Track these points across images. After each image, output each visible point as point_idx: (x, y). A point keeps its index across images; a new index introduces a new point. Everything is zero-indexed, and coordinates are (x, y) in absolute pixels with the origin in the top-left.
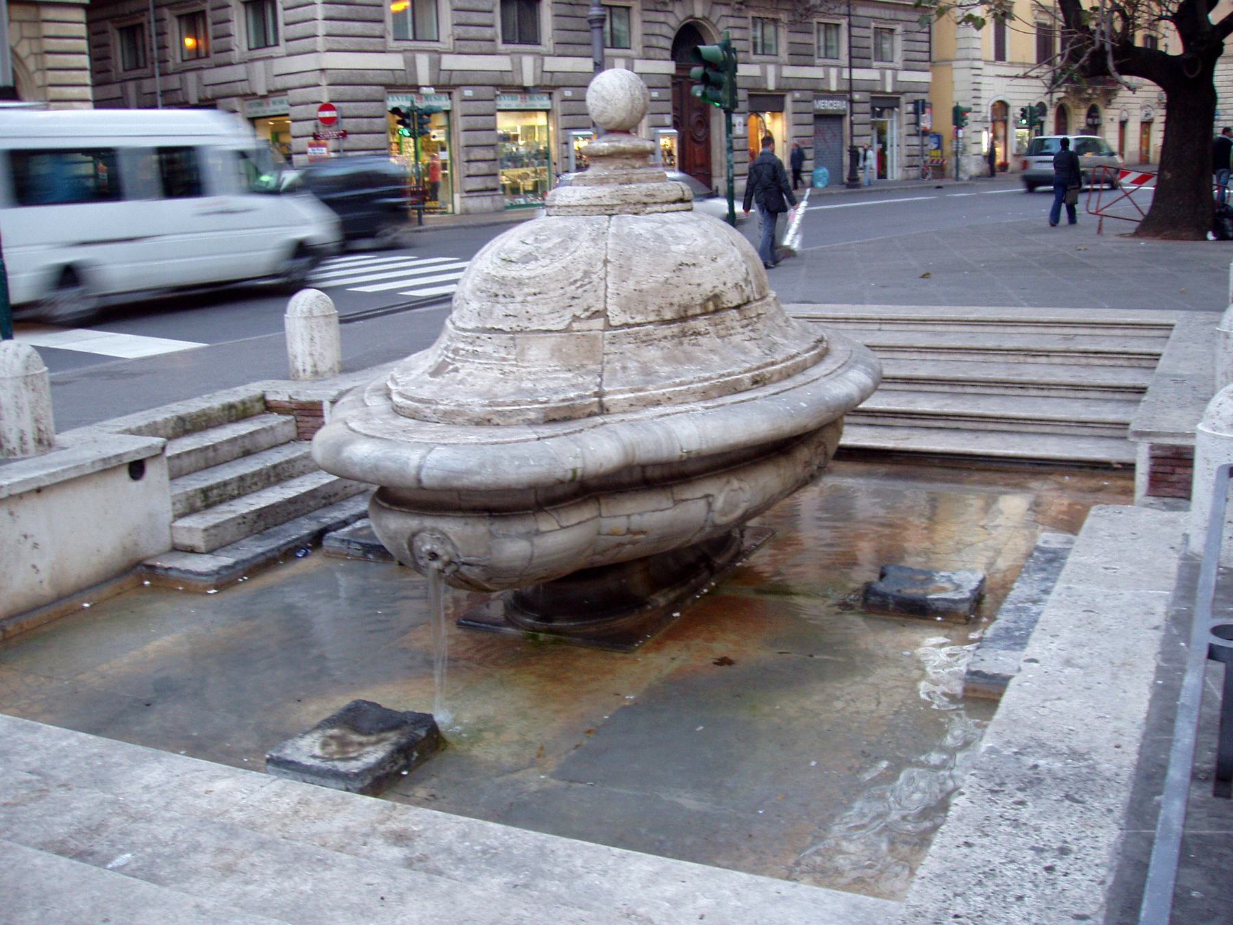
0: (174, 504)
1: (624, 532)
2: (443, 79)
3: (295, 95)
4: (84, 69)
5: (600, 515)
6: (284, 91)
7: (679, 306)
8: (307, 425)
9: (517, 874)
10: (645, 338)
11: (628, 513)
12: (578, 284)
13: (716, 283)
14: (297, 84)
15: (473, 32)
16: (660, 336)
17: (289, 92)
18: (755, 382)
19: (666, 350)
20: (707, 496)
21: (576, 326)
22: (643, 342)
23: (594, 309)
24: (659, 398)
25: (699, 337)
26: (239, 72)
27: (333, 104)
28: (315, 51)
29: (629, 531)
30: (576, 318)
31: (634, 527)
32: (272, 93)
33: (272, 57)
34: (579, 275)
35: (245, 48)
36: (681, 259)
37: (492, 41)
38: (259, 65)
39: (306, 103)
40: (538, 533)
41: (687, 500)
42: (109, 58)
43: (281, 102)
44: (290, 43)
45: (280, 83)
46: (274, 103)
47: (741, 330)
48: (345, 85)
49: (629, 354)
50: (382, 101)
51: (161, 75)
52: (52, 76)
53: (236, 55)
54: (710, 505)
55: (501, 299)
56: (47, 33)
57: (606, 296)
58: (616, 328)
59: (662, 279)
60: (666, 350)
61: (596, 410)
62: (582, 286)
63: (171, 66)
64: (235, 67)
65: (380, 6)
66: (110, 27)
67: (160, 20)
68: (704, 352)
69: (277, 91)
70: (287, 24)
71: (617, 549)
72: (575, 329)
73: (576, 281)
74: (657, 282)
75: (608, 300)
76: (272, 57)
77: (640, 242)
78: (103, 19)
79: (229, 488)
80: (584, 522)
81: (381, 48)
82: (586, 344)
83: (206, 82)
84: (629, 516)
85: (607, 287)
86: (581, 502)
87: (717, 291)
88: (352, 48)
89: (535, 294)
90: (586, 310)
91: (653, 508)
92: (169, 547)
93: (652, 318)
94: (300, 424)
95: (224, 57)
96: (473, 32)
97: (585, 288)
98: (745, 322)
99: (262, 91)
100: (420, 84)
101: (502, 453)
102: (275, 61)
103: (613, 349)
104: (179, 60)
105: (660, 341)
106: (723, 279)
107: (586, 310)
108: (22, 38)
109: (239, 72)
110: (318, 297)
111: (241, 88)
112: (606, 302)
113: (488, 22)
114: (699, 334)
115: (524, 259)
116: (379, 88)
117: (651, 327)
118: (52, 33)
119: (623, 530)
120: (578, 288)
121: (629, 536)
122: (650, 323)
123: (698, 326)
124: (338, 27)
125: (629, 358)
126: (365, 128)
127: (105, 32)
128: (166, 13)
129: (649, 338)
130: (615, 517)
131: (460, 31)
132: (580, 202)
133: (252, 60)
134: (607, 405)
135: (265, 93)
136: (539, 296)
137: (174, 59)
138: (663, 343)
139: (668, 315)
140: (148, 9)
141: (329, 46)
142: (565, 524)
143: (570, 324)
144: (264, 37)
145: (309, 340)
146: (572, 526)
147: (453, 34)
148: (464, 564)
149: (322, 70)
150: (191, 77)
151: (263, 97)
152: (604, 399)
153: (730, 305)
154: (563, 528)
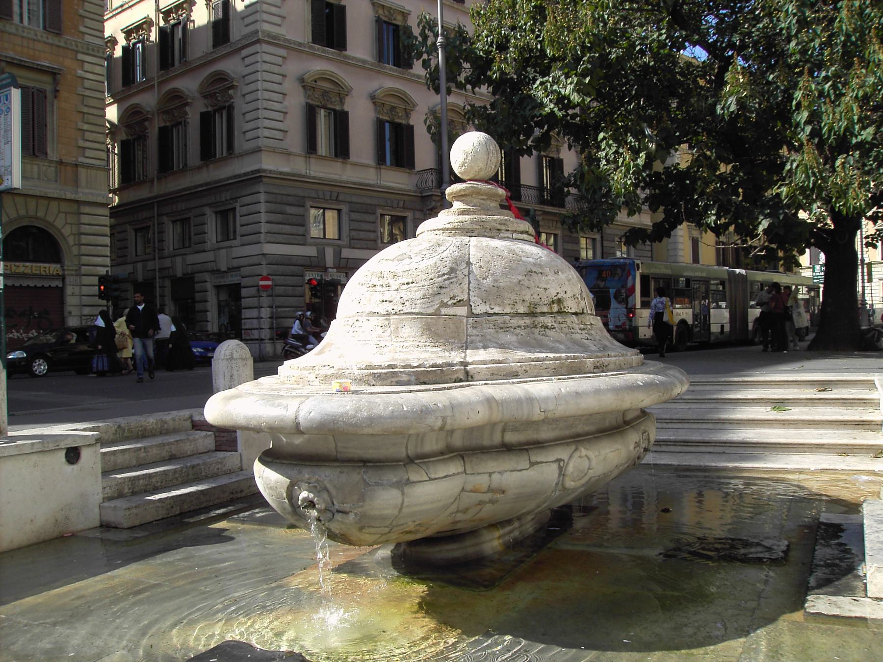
0: (104, 488)
1: (486, 490)
2: (343, 263)
3: (245, 271)
4: (106, 246)
5: (465, 472)
6: (238, 268)
7: (530, 304)
8: (224, 439)
9: (124, 454)
10: (502, 325)
11: (490, 471)
12: (446, 277)
13: (559, 290)
14: (247, 263)
15: (362, 235)
16: (515, 325)
17: (242, 269)
18: (596, 367)
19: (520, 337)
20: (558, 461)
21: (444, 311)
22: (501, 328)
23: (459, 298)
24: (518, 369)
25: (546, 330)
26: (209, 256)
27: (270, 277)
28: (260, 243)
29: (490, 490)
30: (444, 305)
31: (495, 485)
32: (230, 269)
33: (231, 247)
34: (446, 270)
35: (214, 241)
36: (529, 268)
37: (375, 241)
38: (223, 251)
39: (253, 276)
40: (409, 482)
41: (542, 462)
42: (127, 248)
43: (236, 276)
44: (244, 238)
45: (235, 263)
46: (232, 276)
47: (580, 332)
48: (277, 265)
49: (488, 337)
50: (302, 276)
51: (159, 258)
52: (84, 249)
53: (208, 246)
54: (560, 468)
55: (378, 288)
56: (82, 221)
57: (469, 290)
58: (478, 315)
59: (516, 281)
60: (520, 337)
61: (461, 376)
62: (448, 279)
63: (166, 252)
64: (206, 253)
65: (303, 216)
66: (129, 228)
67: (160, 224)
68: (553, 342)
69: (233, 268)
70: (242, 226)
71: (479, 507)
72: (443, 313)
73: (444, 274)
74: (510, 282)
75: (471, 293)
76: (231, 247)
77: (496, 252)
78: (125, 223)
79: (154, 480)
80: (450, 476)
81: (302, 242)
82: (452, 326)
83: (188, 263)
84: (490, 474)
85: (469, 283)
86: (451, 458)
87: (559, 296)
88: (283, 241)
89: (408, 284)
90: (452, 298)
91: (511, 468)
92: (97, 524)
93: (508, 310)
94: (218, 439)
95: (200, 247)
96: (362, 235)
97: (451, 280)
98: (582, 326)
99: (224, 268)
100: (327, 266)
101: (378, 400)
102: (234, 249)
103: (475, 332)
104: (171, 249)
105: (515, 328)
106: (564, 289)
107: (452, 298)
108: (66, 223)
109: (209, 256)
110: (238, 345)
111: (210, 266)
112: (469, 294)
113: (372, 229)
114: (547, 327)
115: (400, 258)
116: (300, 268)
117: (508, 318)
118: (86, 222)
119: (485, 487)
120: (445, 280)
121: (490, 495)
122: (506, 314)
123: (546, 321)
124: (275, 228)
125: (490, 340)
126: (290, 293)
127: (125, 231)
128: (165, 219)
129: (506, 325)
130: (479, 474)
131: (353, 233)
132: (445, 226)
133: (219, 249)
134: (471, 373)
135: (226, 270)
136: (410, 285)
137: (169, 249)
138: (518, 331)
139: (521, 310)
140: (154, 217)
141: (268, 239)
142: (433, 476)
143: (438, 309)
144: (227, 233)
145: (229, 377)
146: (439, 478)
147: (350, 235)
148: (339, 511)
149: (263, 254)
150: (179, 260)
151: (224, 272)
152: (469, 368)
153: (570, 311)
154: (431, 479)
